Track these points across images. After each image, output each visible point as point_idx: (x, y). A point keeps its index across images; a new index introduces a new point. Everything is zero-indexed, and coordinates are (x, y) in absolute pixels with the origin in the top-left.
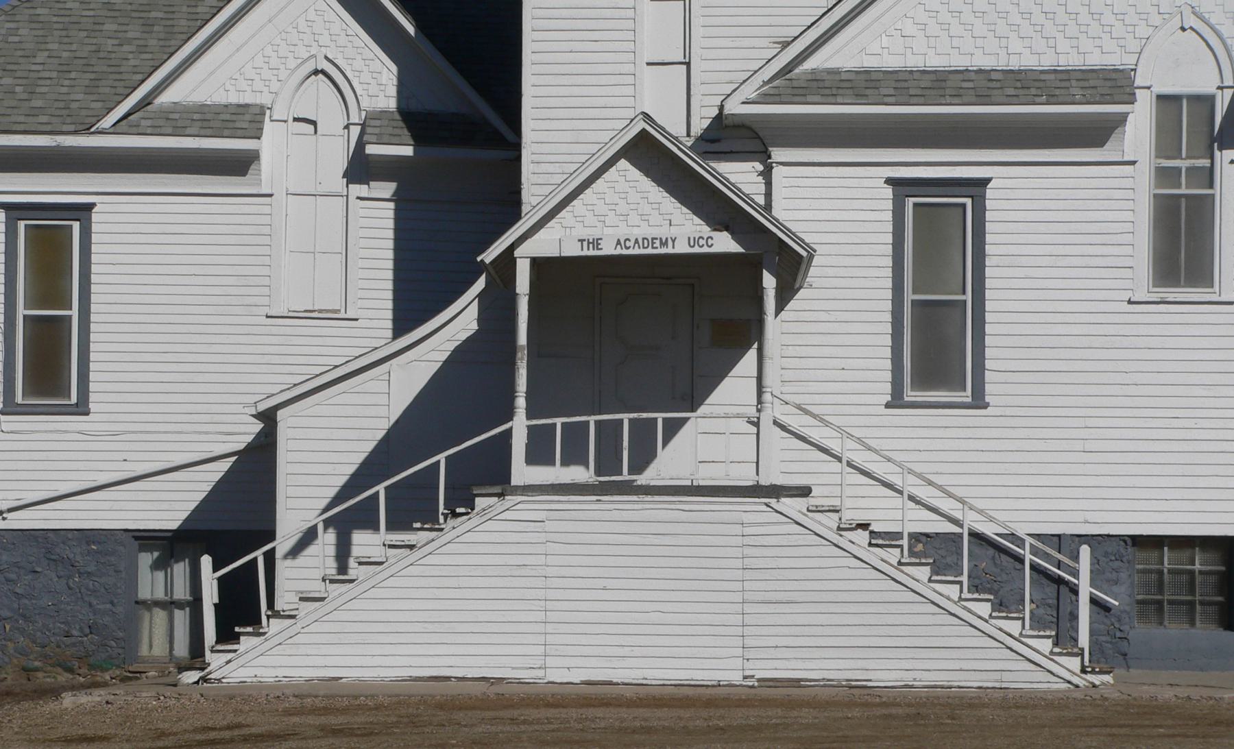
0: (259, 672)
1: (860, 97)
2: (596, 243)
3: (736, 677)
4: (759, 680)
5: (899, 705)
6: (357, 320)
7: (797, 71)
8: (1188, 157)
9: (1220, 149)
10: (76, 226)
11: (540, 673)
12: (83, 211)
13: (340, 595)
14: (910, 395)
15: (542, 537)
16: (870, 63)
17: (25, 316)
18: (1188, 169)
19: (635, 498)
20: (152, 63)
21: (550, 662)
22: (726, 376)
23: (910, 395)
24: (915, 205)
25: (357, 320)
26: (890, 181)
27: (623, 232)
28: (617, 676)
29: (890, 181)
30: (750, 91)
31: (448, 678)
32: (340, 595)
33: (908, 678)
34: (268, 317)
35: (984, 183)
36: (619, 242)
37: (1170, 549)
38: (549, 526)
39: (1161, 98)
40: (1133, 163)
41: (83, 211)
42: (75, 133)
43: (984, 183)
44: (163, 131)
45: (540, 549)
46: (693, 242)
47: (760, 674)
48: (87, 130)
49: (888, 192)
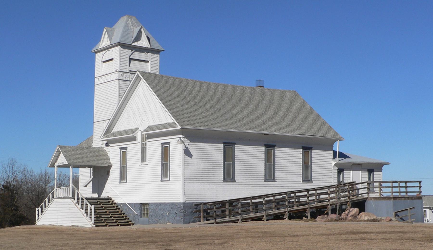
4: (72, 225)
7: (112, 132)
9: (147, 139)
11: (57, 224)
14: (163, 179)
23: (163, 179)
33: (83, 225)
38: (56, 203)
41: (126, 148)
47: (72, 225)
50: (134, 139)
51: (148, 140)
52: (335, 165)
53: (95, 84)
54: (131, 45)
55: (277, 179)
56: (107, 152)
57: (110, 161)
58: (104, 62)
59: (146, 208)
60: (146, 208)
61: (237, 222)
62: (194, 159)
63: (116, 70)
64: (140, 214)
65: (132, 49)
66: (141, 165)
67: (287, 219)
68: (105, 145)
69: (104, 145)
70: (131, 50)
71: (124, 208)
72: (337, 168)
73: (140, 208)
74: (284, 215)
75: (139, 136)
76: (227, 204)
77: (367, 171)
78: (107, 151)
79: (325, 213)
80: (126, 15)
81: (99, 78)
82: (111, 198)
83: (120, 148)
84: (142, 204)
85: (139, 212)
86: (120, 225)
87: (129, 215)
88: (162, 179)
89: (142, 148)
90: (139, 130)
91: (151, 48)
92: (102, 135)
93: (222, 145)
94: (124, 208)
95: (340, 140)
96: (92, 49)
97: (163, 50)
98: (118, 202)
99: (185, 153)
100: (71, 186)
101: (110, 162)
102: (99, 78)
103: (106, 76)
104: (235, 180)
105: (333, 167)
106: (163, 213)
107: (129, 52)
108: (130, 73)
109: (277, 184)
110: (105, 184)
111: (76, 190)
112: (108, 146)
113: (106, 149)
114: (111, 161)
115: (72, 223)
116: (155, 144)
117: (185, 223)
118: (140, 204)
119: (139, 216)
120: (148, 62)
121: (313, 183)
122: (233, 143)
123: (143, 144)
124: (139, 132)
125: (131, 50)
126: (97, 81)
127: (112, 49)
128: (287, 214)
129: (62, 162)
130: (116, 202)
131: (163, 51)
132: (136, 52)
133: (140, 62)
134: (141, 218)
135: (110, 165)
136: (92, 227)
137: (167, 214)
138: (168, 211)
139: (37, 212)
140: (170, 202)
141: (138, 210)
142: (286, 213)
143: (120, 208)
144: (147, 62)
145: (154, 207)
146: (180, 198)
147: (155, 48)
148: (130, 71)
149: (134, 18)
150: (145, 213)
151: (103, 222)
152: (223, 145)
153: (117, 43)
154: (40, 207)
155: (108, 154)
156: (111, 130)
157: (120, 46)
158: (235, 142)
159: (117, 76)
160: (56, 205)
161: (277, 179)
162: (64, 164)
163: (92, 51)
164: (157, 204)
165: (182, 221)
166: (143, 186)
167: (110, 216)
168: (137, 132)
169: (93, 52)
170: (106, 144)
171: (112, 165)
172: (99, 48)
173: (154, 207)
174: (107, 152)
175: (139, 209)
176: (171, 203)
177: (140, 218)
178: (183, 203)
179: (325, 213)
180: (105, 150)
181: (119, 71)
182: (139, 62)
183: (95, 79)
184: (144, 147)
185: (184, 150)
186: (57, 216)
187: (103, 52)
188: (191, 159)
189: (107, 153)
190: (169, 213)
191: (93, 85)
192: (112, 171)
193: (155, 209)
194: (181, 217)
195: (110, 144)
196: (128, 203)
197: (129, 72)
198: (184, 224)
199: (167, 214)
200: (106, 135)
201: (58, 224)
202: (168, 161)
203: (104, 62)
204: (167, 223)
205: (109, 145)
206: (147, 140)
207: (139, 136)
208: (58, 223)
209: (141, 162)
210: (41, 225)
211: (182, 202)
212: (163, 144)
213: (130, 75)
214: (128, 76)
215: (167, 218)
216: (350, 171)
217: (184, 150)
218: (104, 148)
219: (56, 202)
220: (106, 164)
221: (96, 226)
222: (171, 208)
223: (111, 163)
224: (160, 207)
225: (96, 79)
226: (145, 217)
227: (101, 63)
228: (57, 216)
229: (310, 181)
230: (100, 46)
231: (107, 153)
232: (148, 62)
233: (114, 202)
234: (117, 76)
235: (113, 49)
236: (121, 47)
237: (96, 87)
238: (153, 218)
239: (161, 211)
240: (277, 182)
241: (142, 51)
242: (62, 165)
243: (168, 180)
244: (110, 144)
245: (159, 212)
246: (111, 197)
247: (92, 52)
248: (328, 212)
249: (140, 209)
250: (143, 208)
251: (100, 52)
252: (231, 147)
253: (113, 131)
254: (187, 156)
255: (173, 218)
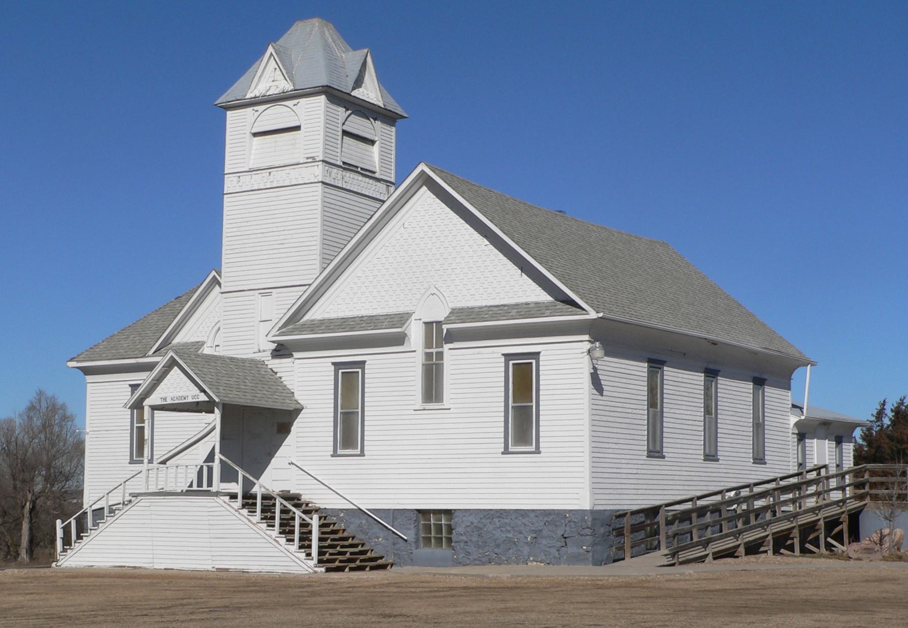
0: (71, 563)
1: (313, 331)
2: (165, 399)
3: (210, 568)
4: (217, 569)
5: (224, 579)
6: (449, 409)
7: (301, 321)
8: (436, 348)
9: (445, 344)
10: (534, 362)
11: (152, 565)
12: (362, 364)
13: (850, 502)
14: (339, 452)
15: (149, 513)
16: (327, 316)
17: (137, 427)
18: (436, 353)
19: (174, 497)
20: (163, 328)
21: (155, 561)
22: (281, 446)
23: (339, 452)
24: (343, 373)
25: (449, 409)
26: (333, 364)
27: (172, 395)
28: (175, 567)
29: (333, 364)
30: (274, 332)
31: (124, 567)
32: (850, 502)
33: (260, 568)
34: (415, 410)
35: (364, 362)
36: (172, 399)
37: (444, 514)
38: (152, 508)
39: (425, 323)
40: (415, 351)
41: (362, 364)
42: (142, 357)
43: (364, 362)
44: (498, 318)
45: (149, 517)
46: (194, 397)
47: (216, 567)
48: (144, 356)
49: (333, 368)
50: (399, 340)
51: (447, 345)
52: (797, 425)
53: (225, 192)
54: (349, 94)
55: (670, 450)
56: (276, 373)
57: (294, 396)
58: (255, 135)
59: (434, 524)
60: (434, 524)
61: (703, 562)
62: (121, 402)
63: (313, 158)
64: (416, 538)
65: (347, 106)
66: (424, 410)
67: (770, 552)
68: (271, 354)
69: (269, 353)
70: (345, 108)
71: (351, 523)
72: (797, 432)
73: (414, 523)
74: (761, 545)
75: (416, 333)
76: (694, 515)
77: (834, 439)
78: (275, 370)
79: (809, 539)
80: (315, 17)
81: (239, 177)
82: (300, 495)
83: (334, 364)
84: (419, 511)
85: (414, 533)
86: (347, 569)
87: (374, 540)
88: (335, 450)
89: (423, 365)
90: (413, 317)
91: (386, 109)
92: (277, 328)
93: (646, 365)
94: (351, 523)
95: (811, 365)
96: (218, 98)
97: (407, 116)
98: (327, 507)
99: (592, 384)
100: (217, 461)
101: (296, 400)
102: (239, 177)
103: (270, 173)
104: (664, 454)
105: (792, 430)
106: (510, 535)
107: (341, 112)
108: (345, 169)
109: (719, 466)
110: (271, 459)
111: (240, 472)
112: (290, 358)
113: (280, 366)
114: (297, 397)
115: (214, 562)
116: (480, 356)
117: (598, 563)
118: (415, 512)
119: (413, 545)
120: (372, 142)
121: (767, 466)
122: (660, 361)
123: (429, 356)
124: (412, 323)
125: (345, 110)
126: (230, 184)
127: (295, 101)
128: (769, 540)
129: (184, 394)
130: (317, 505)
131: (405, 119)
132: (353, 116)
133: (359, 142)
134: (418, 550)
135: (298, 406)
136: (315, 572)
137: (529, 540)
138: (535, 532)
139: (59, 533)
140: (381, 508)
141: (409, 529)
142: (767, 539)
143: (336, 523)
144: (371, 143)
145: (475, 521)
146: (578, 499)
147: (393, 110)
148: (344, 163)
149: (331, 25)
150: (430, 538)
151: (325, 559)
152: (647, 364)
153: (322, 86)
154: (74, 519)
155: (281, 378)
156: (299, 318)
157: (326, 96)
158: (665, 360)
159: (318, 172)
160: (149, 513)
161: (670, 450)
162: (190, 400)
163: (216, 103)
164: (487, 513)
165: (591, 559)
166: (422, 466)
167: (327, 545)
168: (409, 324)
169: (220, 106)
170: (275, 350)
171: (303, 408)
172: (246, 96)
173: (475, 521)
174: (276, 373)
175: (412, 526)
176: (544, 510)
177: (416, 549)
178: (592, 512)
179: (809, 539)
180: (269, 367)
181: (323, 161)
182: (356, 141)
183: (224, 177)
184: (433, 364)
185: (591, 373)
186: (150, 543)
187: (256, 108)
188: (600, 397)
189: (278, 375)
190: (534, 535)
191: (219, 194)
192: (300, 425)
193: (481, 525)
194: (585, 548)
195: (293, 353)
196: (367, 510)
197: (341, 164)
198: (594, 565)
199: (529, 540)
200: (285, 327)
201: (155, 564)
202: (531, 402)
203: (255, 135)
204: (529, 564)
205: (292, 356)
206: (447, 347)
207: (416, 333)
208: (155, 561)
209: (423, 403)
210: (82, 567)
211: (588, 509)
212: (508, 357)
213: (344, 173)
214: (340, 177)
215: (526, 550)
216: (813, 440)
217: (591, 373)
218: (263, 361)
219: (152, 504)
220: (291, 405)
221: (328, 570)
222: (543, 524)
223: (299, 403)
224: (499, 521)
225: (230, 179)
226: (432, 546)
227: (248, 135)
228: (150, 543)
229: (762, 461)
230: (250, 91)
231: (278, 375)
232: (372, 142)
233: (310, 505)
234: (318, 172)
235: (298, 103)
236: (328, 99)
237: (226, 199)
238: (471, 549)
239: (501, 531)
240: (720, 462)
241: (363, 113)
242: (175, 404)
243: (359, 453)
244: (293, 353)
245: (494, 534)
246: (301, 492)
247: (216, 105)
248: (818, 536)
249: (416, 524)
250: (423, 524)
251: (246, 108)
252: (657, 370)
253: (306, 318)
254: (595, 390)
255: (553, 551)
